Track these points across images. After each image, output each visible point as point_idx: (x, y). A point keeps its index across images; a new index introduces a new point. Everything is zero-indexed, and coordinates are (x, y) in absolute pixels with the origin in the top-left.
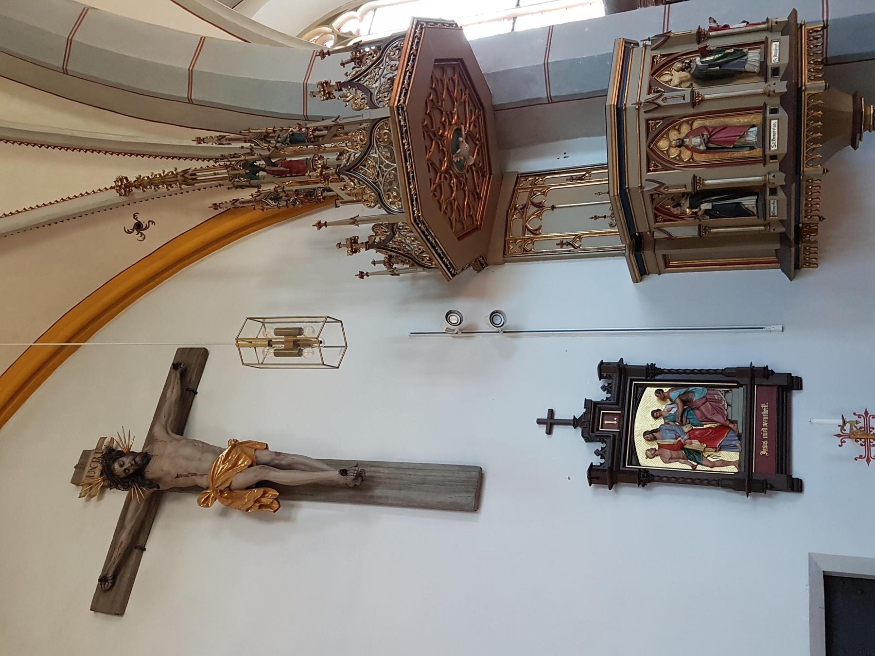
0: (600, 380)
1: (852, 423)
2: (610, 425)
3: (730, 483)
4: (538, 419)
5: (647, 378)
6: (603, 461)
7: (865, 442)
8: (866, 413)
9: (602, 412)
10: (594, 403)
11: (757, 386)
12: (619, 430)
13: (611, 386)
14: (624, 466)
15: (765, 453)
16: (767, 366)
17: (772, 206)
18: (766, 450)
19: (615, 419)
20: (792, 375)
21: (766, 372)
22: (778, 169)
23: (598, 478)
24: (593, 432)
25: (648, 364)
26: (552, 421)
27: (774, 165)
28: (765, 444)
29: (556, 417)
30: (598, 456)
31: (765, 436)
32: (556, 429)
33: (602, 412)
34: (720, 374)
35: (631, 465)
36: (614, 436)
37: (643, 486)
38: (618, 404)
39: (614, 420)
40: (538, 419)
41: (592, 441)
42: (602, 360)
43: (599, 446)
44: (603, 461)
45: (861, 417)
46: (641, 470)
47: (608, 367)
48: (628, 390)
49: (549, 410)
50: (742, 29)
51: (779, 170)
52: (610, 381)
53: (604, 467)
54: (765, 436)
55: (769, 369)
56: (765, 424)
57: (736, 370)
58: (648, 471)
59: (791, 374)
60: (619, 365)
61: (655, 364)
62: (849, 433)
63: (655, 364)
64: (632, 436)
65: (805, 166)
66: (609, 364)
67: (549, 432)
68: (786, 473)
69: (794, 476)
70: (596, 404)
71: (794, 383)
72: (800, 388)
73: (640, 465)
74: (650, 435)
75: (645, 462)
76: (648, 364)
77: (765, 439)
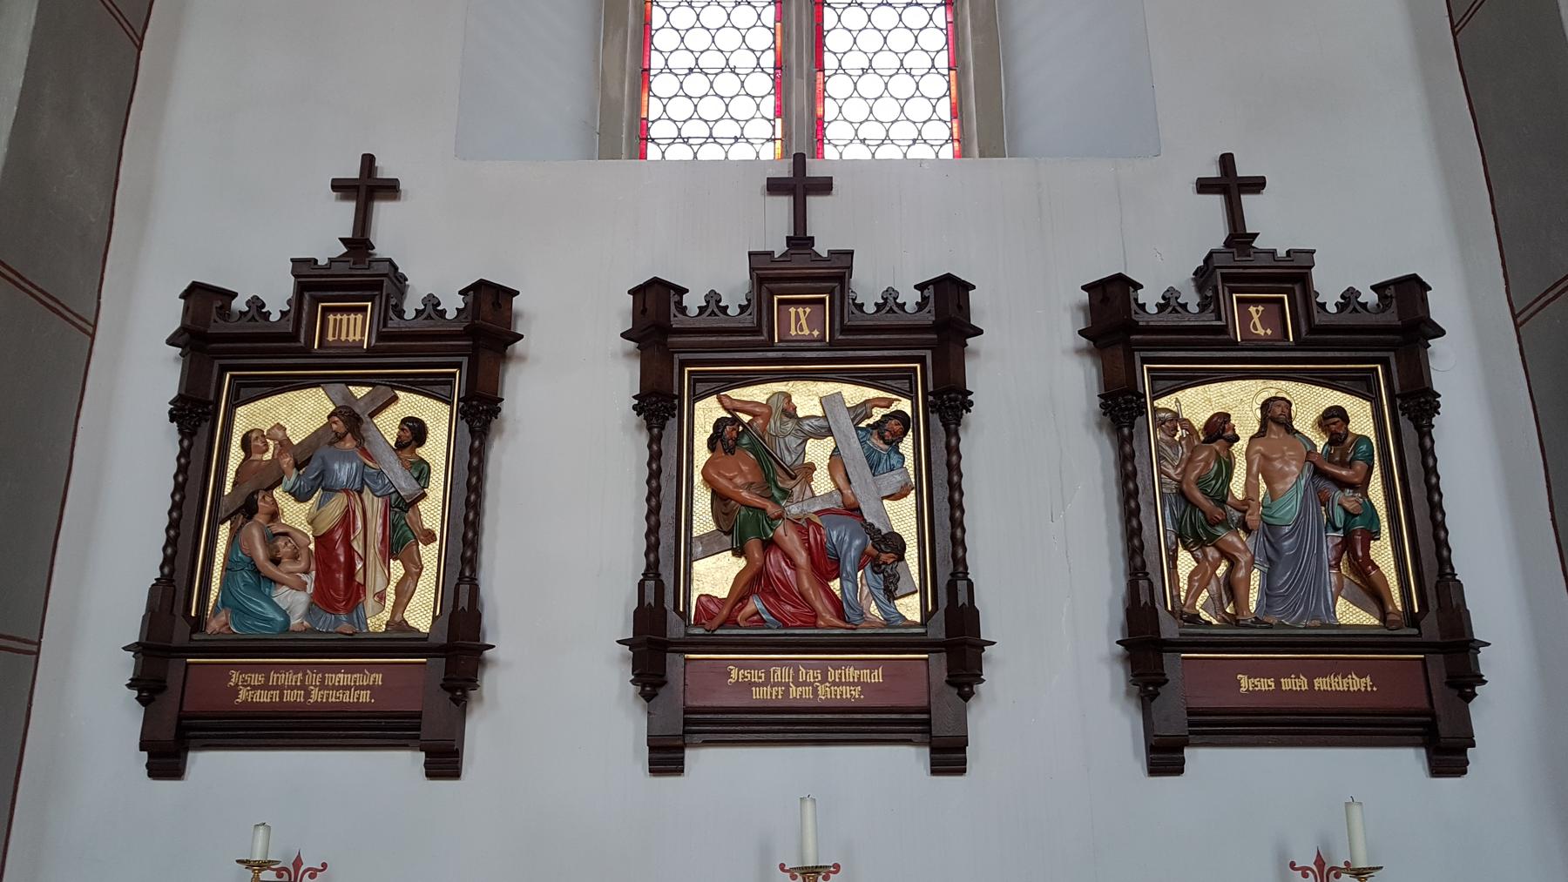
0: (1084, 288)
2: (801, 323)
3: (1144, 598)
4: (333, 180)
5: (931, 394)
6: (1152, 309)
10: (1307, 273)
11: (927, 660)
12: (1239, 340)
13: (432, 318)
14: (1145, 360)
15: (1243, 685)
18: (741, 676)
19: (1269, 332)
21: (1466, 680)
25: (971, 393)
26: (800, 191)
28: (1266, 684)
29: (1246, 200)
30: (1164, 298)
32: (1216, 201)
33: (1285, 296)
35: (1153, 379)
36: (1223, 330)
40: (333, 180)
43: (1191, 299)
44: (1152, 309)
46: (1143, 400)
48: (886, 353)
53: (215, 321)
54: (1287, 684)
55: (1478, 689)
57: (1458, 605)
58: (1141, 414)
61: (1439, 414)
63: (1439, 414)
64: (1227, 375)
68: (1191, 733)
69: (1187, 752)
72: (1437, 770)
76: (971, 393)
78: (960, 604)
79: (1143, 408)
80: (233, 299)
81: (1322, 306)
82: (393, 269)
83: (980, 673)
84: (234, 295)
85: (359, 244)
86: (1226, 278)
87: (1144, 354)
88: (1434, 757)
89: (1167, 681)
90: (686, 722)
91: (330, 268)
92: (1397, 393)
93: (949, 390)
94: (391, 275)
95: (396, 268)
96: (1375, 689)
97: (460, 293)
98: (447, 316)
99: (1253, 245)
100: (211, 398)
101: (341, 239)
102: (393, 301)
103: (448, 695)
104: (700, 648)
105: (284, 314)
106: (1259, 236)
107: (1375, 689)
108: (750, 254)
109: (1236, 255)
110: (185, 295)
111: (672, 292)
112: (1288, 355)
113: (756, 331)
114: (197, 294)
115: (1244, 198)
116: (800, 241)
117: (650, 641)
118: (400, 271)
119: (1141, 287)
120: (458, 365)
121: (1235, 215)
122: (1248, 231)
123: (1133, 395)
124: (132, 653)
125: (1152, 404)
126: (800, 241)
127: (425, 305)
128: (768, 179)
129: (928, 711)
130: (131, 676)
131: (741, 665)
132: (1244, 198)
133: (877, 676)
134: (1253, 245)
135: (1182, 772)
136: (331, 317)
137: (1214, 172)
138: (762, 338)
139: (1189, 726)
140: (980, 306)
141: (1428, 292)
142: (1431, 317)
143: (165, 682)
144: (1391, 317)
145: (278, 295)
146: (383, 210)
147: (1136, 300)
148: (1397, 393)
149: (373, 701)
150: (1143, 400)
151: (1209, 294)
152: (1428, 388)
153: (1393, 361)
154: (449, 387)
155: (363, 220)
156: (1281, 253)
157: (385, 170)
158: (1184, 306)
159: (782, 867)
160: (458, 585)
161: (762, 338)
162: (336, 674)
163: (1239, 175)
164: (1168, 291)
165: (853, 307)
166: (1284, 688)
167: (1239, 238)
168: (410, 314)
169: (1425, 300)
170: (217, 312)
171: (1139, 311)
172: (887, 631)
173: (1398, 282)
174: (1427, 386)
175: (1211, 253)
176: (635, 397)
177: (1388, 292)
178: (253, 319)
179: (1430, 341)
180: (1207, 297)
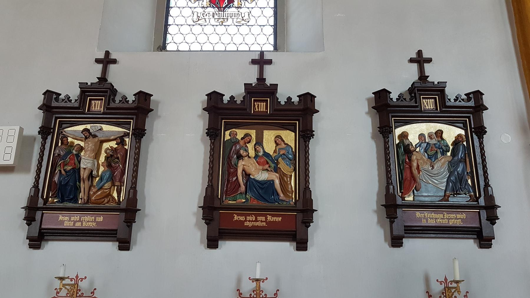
0: (373, 93)
1: (457, 289)
6: (395, 100)
9: (437, 96)
10: (444, 89)
11: (296, 215)
14: (393, 117)
18: (237, 218)
21: (493, 219)
23: (211, 99)
24: (418, 90)
29: (426, 65)
32: (256, 67)
35: (395, 122)
42: (484, 94)
43: (408, 97)
44: (395, 100)
45: (91, 293)
47: (479, 99)
48: (411, 114)
49: (106, 51)
50: (475, 205)
53: (448, 102)
55: (311, 224)
62: (449, 286)
73: (395, 129)
74: (439, 133)
77: (246, 218)
78: (490, 195)
79: (392, 132)
80: (60, 96)
81: (449, 100)
82: (112, 87)
83: (312, 219)
84: (60, 95)
85: (103, 79)
86: (418, 90)
87: (393, 114)
89: (35, 220)
90: (219, 233)
91: (91, 86)
92: (472, 127)
93: (386, 126)
94: (111, 89)
95: (113, 87)
96: (267, 225)
97: (134, 95)
98: (237, 102)
99: (427, 80)
100: (52, 127)
101: (97, 78)
102: (112, 97)
104: (232, 210)
105: (76, 100)
106: (429, 77)
107: (267, 225)
108: (245, 84)
109: (422, 83)
110: (44, 94)
111: (54, 94)
112: (105, 116)
113: (417, 107)
114: (48, 94)
115: (425, 64)
116: (261, 80)
117: (208, 206)
118: (114, 88)
119: (391, 93)
120: (132, 119)
121: (421, 70)
122: (426, 75)
123: (388, 127)
124: (202, 209)
125: (130, 132)
126: (261, 80)
127: (122, 99)
128: (252, 59)
129: (296, 231)
130: (24, 217)
131: (238, 215)
132: (425, 64)
133: (101, 219)
134: (427, 80)
135: (307, 250)
136: (93, 102)
137: (414, 56)
138: (418, 109)
139: (116, 236)
140: (318, 104)
141: (483, 96)
142: (484, 104)
143: (35, 218)
144: (472, 103)
145: (74, 93)
146: (112, 67)
147: (390, 97)
148: (472, 127)
149: (96, 226)
150: (392, 129)
151: (413, 95)
152: (483, 126)
153: (472, 118)
154: (129, 125)
155: (105, 71)
156: (436, 83)
157: (425, 55)
158: (405, 99)
159: (437, 280)
160: (130, 190)
161: (418, 109)
162: (260, 217)
163: (423, 57)
164: (458, 95)
165: (389, 99)
166: (265, 223)
167: (423, 77)
168: (117, 101)
169: (482, 99)
170: (112, 100)
171: (390, 100)
172: (414, 202)
173: (474, 93)
174: (482, 125)
175: (414, 83)
176: (206, 129)
177: (470, 96)
178: (123, 102)
179: (483, 111)
180: (412, 96)
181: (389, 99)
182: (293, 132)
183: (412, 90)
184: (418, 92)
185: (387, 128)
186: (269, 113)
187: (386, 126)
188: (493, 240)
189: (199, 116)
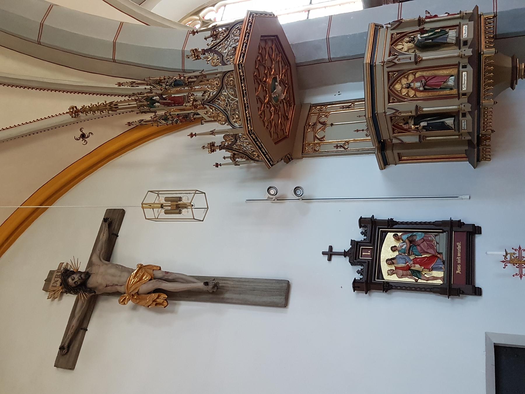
0: (360, 228)
1: (511, 254)
2: (366, 255)
5: (388, 227)
6: (362, 277)
7: (519, 265)
8: (520, 248)
9: (361, 247)
10: (356, 242)
11: (454, 232)
12: (371, 258)
13: (367, 232)
14: (374, 280)
15: (459, 272)
16: (460, 220)
17: (463, 124)
19: (369, 252)
20: (475, 225)
21: (460, 224)
22: (467, 102)
23: (359, 287)
25: (389, 219)
26: (331, 253)
27: (464, 99)
28: (459, 267)
29: (334, 250)
30: (359, 274)
31: (459, 262)
32: (334, 258)
33: (361, 247)
34: (432, 224)
35: (379, 279)
36: (369, 262)
37: (386, 292)
38: (371, 243)
39: (369, 253)
41: (355, 265)
42: (361, 216)
43: (359, 268)
44: (362, 277)
45: (516, 251)
46: (385, 282)
47: (365, 220)
48: (377, 234)
49: (329, 246)
51: (468, 102)
52: (366, 229)
53: (362, 280)
54: (459, 262)
55: (462, 221)
56: (459, 255)
57: (442, 222)
58: (389, 283)
59: (474, 225)
60: (371, 219)
61: (393, 219)
62: (509, 260)
63: (393, 219)
64: (379, 262)
65: (483, 100)
66: (365, 218)
67: (330, 259)
70: (357, 242)
71: (476, 230)
72: (480, 233)
73: (384, 279)
74: (390, 261)
75: (387, 277)
76: (389, 219)
77: (459, 264)
88: (477, 233)
103: (462, 226)
181: (361, 281)
182: (387, 233)
183: (353, 263)
184: (357, 259)
185: (385, 286)
186: (372, 247)
187: (383, 287)
188: (475, 225)
189: (370, 295)
